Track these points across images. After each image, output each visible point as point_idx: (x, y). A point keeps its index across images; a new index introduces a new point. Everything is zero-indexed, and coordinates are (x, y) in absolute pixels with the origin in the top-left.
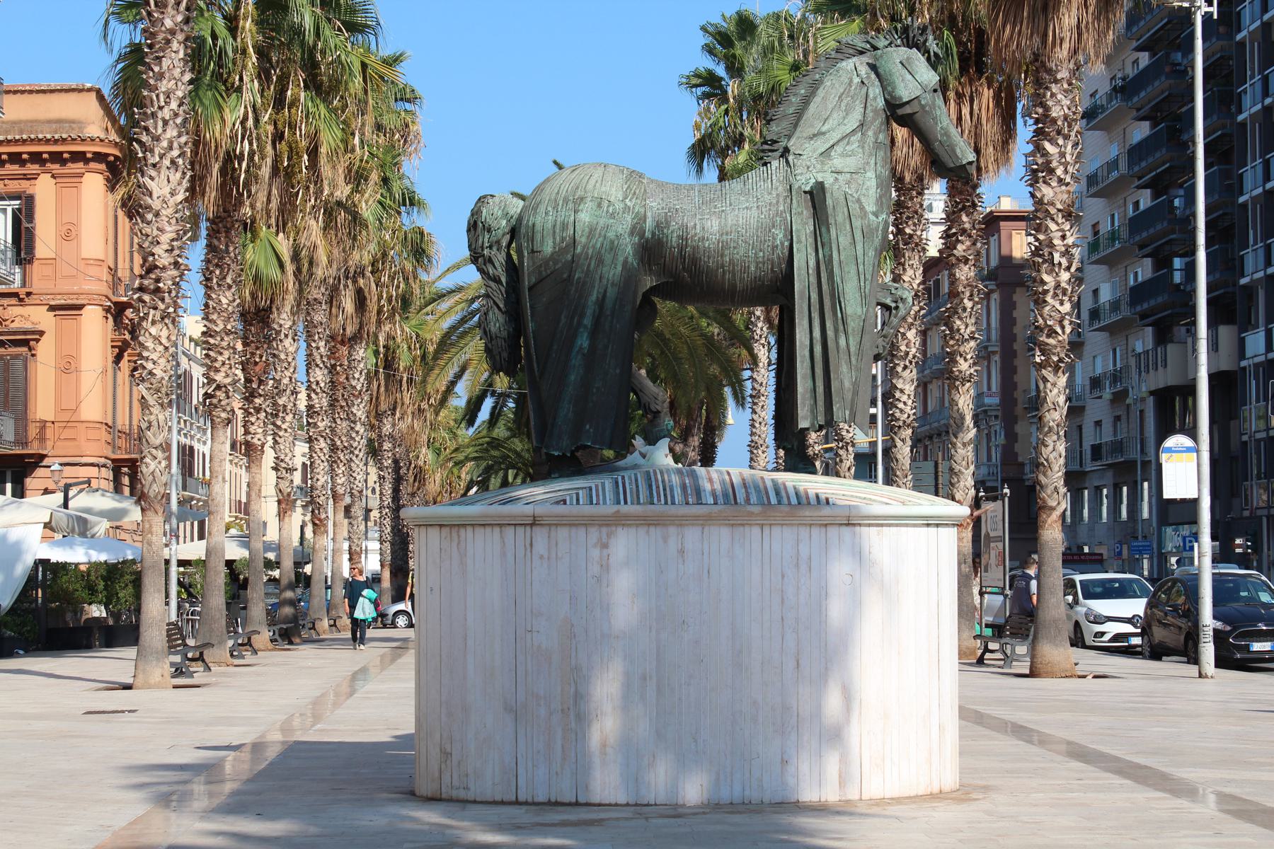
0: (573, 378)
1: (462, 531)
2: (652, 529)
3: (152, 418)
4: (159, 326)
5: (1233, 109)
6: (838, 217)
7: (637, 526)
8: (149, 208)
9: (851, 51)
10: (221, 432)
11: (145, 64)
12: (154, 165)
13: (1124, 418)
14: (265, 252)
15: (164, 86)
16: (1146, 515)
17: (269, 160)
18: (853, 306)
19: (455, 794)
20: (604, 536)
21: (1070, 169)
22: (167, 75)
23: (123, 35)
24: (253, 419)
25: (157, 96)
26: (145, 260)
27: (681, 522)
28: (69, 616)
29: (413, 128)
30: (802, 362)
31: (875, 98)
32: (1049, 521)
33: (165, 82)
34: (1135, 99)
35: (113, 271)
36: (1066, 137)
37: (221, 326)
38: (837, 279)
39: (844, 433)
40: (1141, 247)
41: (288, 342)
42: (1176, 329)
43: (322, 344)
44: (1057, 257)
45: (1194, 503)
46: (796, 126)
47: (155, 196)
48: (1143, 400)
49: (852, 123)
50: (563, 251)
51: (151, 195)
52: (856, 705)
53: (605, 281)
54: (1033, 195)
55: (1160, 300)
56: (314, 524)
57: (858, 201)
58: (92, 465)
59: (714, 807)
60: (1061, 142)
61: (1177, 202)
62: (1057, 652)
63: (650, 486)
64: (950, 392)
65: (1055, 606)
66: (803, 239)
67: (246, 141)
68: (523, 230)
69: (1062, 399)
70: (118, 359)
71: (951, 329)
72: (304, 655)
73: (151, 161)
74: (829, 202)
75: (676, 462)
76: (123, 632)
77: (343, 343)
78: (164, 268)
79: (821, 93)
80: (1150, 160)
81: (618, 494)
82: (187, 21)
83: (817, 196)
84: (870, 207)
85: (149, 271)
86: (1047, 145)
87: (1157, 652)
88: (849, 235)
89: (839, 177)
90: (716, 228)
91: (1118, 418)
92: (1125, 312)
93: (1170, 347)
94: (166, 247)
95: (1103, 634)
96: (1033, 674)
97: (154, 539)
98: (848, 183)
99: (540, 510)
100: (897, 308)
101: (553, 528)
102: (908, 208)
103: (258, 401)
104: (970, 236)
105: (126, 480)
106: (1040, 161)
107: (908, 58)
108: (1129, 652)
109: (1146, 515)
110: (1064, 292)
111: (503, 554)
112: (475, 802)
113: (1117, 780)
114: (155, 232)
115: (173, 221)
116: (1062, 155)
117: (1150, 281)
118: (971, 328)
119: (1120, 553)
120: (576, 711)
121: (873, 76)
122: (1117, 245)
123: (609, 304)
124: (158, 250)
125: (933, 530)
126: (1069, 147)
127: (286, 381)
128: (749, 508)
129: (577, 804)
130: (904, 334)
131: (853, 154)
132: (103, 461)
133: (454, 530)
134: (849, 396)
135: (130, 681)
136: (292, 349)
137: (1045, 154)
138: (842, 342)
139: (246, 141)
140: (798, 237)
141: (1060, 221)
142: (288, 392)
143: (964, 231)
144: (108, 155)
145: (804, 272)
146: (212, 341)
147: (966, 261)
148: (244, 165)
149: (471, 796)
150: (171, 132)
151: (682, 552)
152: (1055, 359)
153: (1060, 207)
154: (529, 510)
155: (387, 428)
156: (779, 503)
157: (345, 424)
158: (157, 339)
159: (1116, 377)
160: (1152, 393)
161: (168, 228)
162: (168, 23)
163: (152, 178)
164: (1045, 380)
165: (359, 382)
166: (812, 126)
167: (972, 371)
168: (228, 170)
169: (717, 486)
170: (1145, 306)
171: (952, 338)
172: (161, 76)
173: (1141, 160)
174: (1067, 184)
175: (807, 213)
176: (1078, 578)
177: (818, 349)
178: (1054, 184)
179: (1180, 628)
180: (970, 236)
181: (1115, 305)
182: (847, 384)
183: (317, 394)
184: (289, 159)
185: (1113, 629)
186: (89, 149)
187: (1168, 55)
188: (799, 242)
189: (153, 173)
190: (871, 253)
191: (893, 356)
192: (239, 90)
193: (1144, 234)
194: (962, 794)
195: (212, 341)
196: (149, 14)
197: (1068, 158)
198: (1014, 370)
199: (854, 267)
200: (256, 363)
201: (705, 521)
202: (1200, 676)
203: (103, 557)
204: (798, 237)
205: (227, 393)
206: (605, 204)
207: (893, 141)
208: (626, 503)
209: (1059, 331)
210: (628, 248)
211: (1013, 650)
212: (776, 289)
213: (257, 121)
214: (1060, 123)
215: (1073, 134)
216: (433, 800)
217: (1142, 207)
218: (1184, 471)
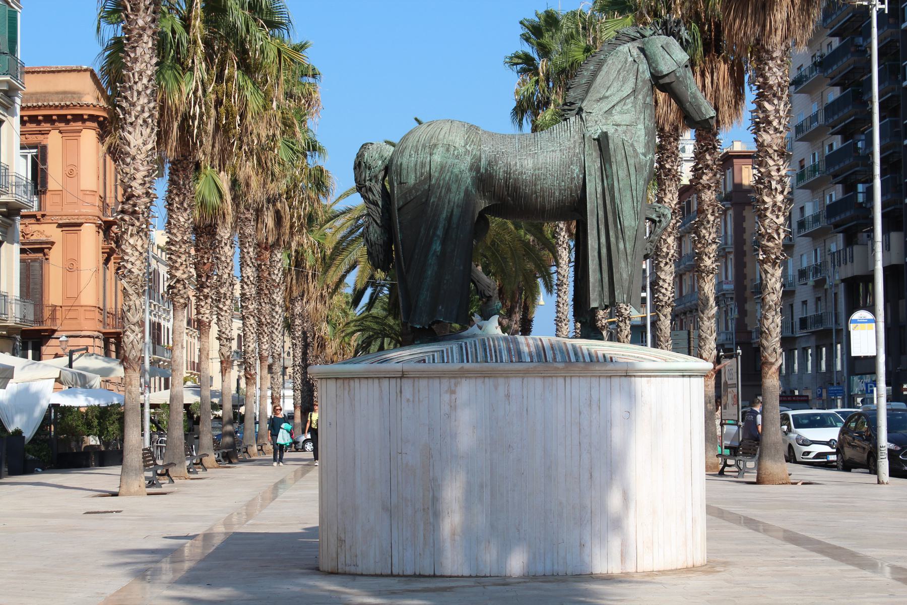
0: (429, 273)
1: (352, 382)
2: (487, 380)
3: (131, 303)
4: (136, 238)
5: (900, 77)
6: (618, 157)
7: (476, 377)
8: (128, 154)
9: (626, 39)
10: (180, 313)
11: (124, 52)
12: (131, 124)
13: (823, 299)
14: (212, 184)
15: (138, 67)
16: (839, 368)
17: (213, 120)
18: (629, 220)
19: (347, 569)
20: (453, 385)
21: (783, 121)
22: (140, 60)
23: (110, 32)
24: (203, 304)
25: (133, 74)
26: (125, 191)
27: (507, 375)
28: (73, 444)
29: (314, 95)
30: (593, 260)
31: (644, 72)
32: (770, 373)
33: (138, 64)
34: (830, 71)
35: (103, 199)
36: (780, 99)
37: (180, 238)
38: (618, 201)
39: (623, 311)
40: (835, 176)
41: (227, 248)
42: (859, 235)
43: (251, 250)
44: (774, 184)
45: (873, 359)
46: (587, 92)
47: (132, 145)
48: (836, 286)
49: (627, 89)
50: (422, 183)
51: (129, 145)
52: (632, 506)
53: (452, 204)
54: (756, 140)
55: (848, 214)
56: (247, 378)
57: (632, 145)
58: (89, 337)
59: (530, 578)
60: (776, 102)
61: (860, 144)
62: (776, 466)
63: (485, 350)
64: (698, 281)
65: (774, 433)
66: (593, 173)
67: (197, 106)
68: (394, 168)
69: (778, 286)
70: (107, 261)
71: (699, 236)
72: (240, 471)
73: (129, 120)
74: (611, 146)
75: (504, 333)
76: (110, 455)
77: (266, 249)
78: (139, 197)
79: (605, 68)
80: (841, 114)
81: (462, 355)
82: (153, 21)
83: (602, 142)
84: (641, 149)
85: (128, 199)
86: (766, 105)
87: (847, 466)
88: (626, 169)
89: (618, 128)
90: (531, 165)
91: (818, 299)
92: (823, 223)
93: (855, 248)
94: (140, 181)
95: (809, 453)
96: (759, 482)
97: (133, 389)
98: (625, 132)
99: (407, 367)
100: (660, 221)
101: (416, 380)
102: (667, 150)
103: (205, 290)
104: (712, 170)
105: (113, 348)
106: (761, 116)
107: (667, 44)
108: (828, 466)
109: (839, 368)
110: (779, 209)
111: (381, 398)
112: (362, 575)
113: (820, 557)
114: (133, 171)
115: (145, 163)
116: (777, 111)
117: (841, 200)
118: (713, 235)
119: (821, 395)
120: (432, 510)
121: (642, 56)
122: (817, 175)
123: (455, 220)
124: (134, 184)
125: (686, 379)
126: (782, 106)
127: (226, 276)
128: (556, 365)
129: (434, 576)
130: (665, 240)
131: (628, 112)
132: (96, 334)
133: (346, 382)
134: (626, 284)
135: (117, 490)
136: (230, 254)
137: (765, 111)
138: (621, 246)
139: (197, 106)
140: (589, 171)
141: (776, 158)
142: (227, 284)
143: (707, 166)
144: (99, 116)
145: (594, 196)
146: (173, 248)
147: (709, 187)
148: (196, 123)
149: (359, 571)
150: (143, 100)
151: (508, 396)
152: (773, 257)
153: (776, 148)
154: (399, 367)
155: (298, 309)
156: (577, 361)
157: (268, 306)
158: (134, 247)
159: (817, 269)
160: (843, 281)
161: (141, 168)
162: (141, 22)
163: (130, 133)
164: (766, 272)
165: (277, 276)
166: (598, 92)
167: (714, 266)
168: (185, 129)
169: (533, 349)
170: (838, 218)
171: (700, 243)
172: (135, 60)
173: (834, 114)
174: (781, 132)
175: (595, 154)
176: (791, 413)
177: (604, 251)
178: (771, 132)
179: (864, 448)
180: (712, 170)
181: (816, 218)
182: (625, 276)
183: (248, 285)
184: (226, 119)
185: (816, 449)
186: (86, 112)
187: (853, 39)
188: (590, 175)
189: (131, 129)
190: (642, 182)
191: (658, 255)
192: (191, 69)
193: (837, 168)
194: (709, 568)
195: (173, 248)
196: (127, 16)
197: (781, 113)
198: (744, 265)
199: (629, 192)
200: (205, 264)
201: (525, 374)
202: (879, 483)
203: (96, 403)
204: (589, 171)
205: (184, 285)
206: (452, 149)
207: (656, 102)
208: (468, 361)
209: (776, 237)
210: (468, 179)
211: (745, 465)
212: (574, 209)
213: (204, 91)
214: (775, 88)
215: (785, 96)
216: (332, 573)
217: (835, 148)
218: (866, 336)
